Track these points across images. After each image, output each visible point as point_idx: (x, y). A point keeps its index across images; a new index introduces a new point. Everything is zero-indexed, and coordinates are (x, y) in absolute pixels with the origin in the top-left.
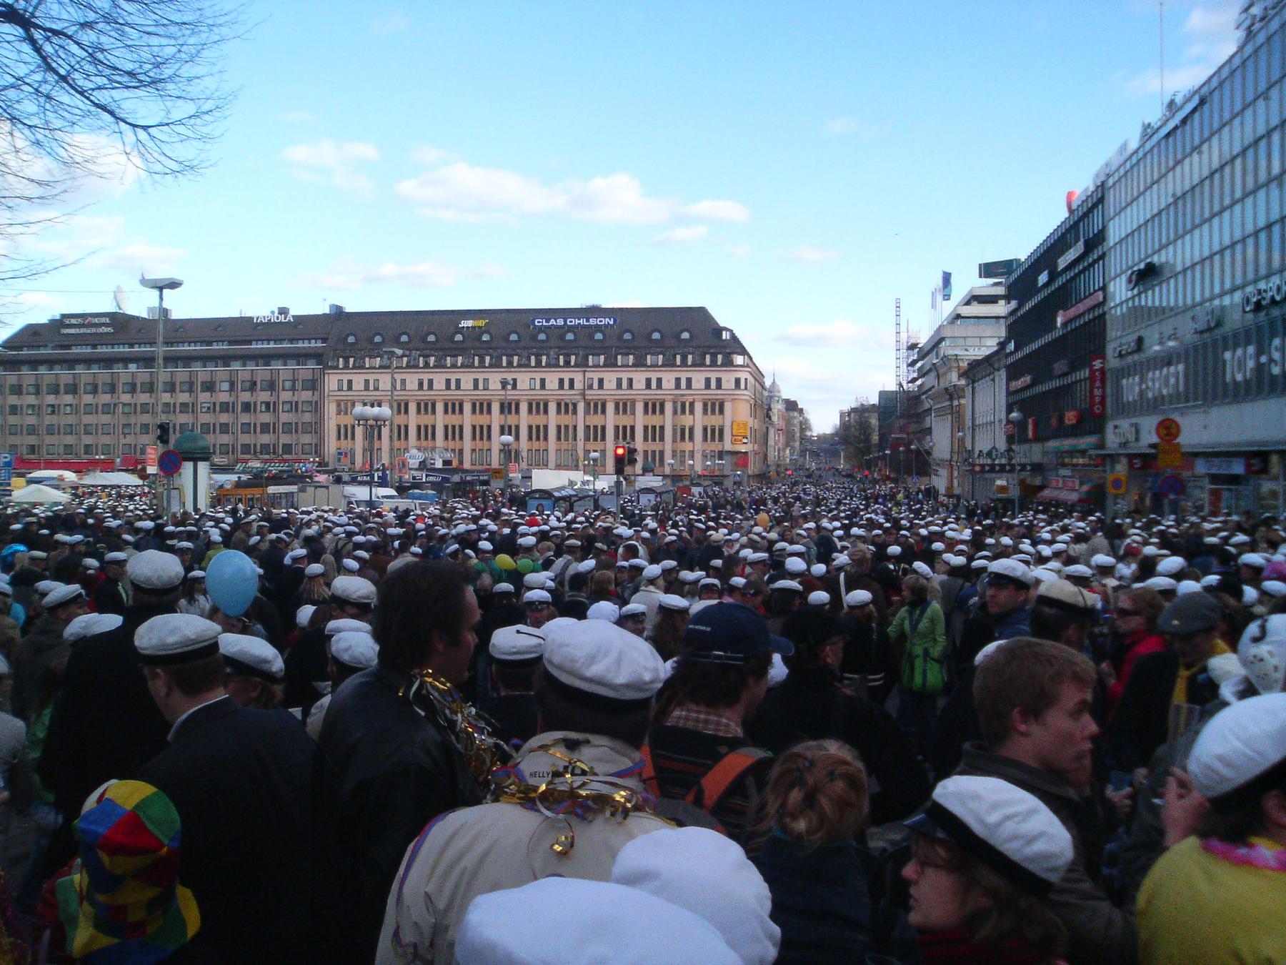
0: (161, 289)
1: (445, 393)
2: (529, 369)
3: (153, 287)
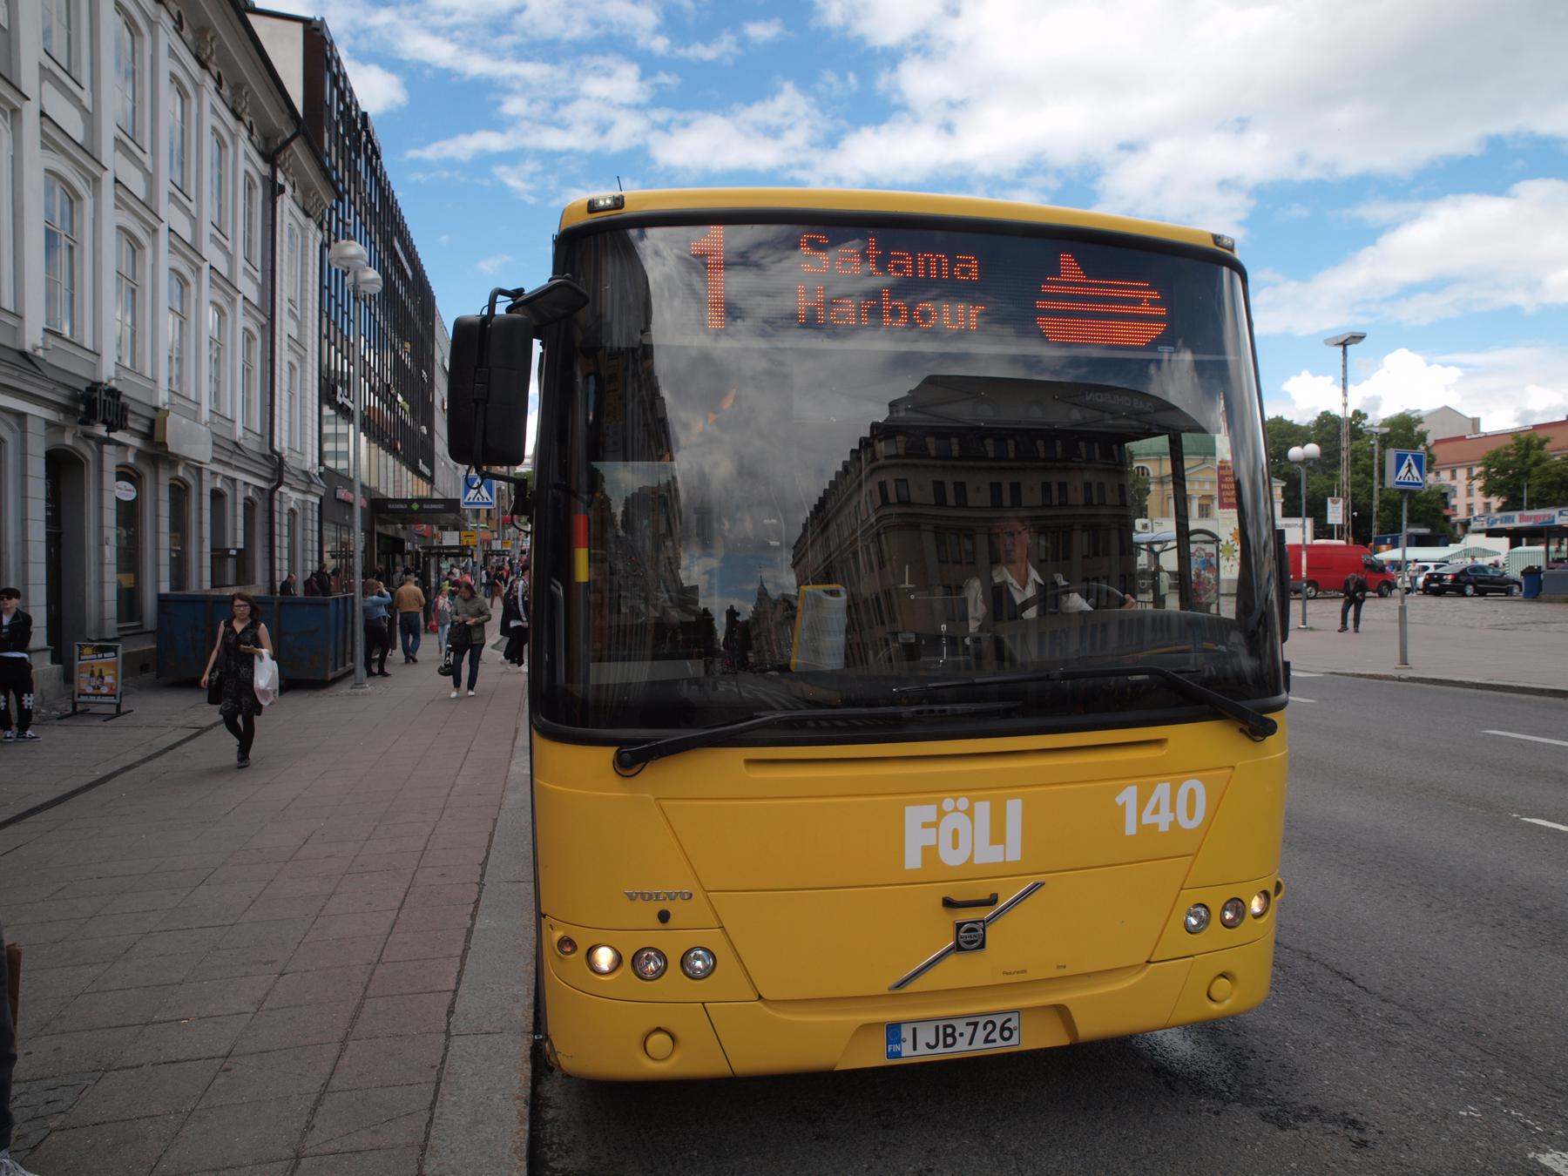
0: (1344, 344)
1: (933, 512)
2: (925, 462)
3: (1337, 344)
